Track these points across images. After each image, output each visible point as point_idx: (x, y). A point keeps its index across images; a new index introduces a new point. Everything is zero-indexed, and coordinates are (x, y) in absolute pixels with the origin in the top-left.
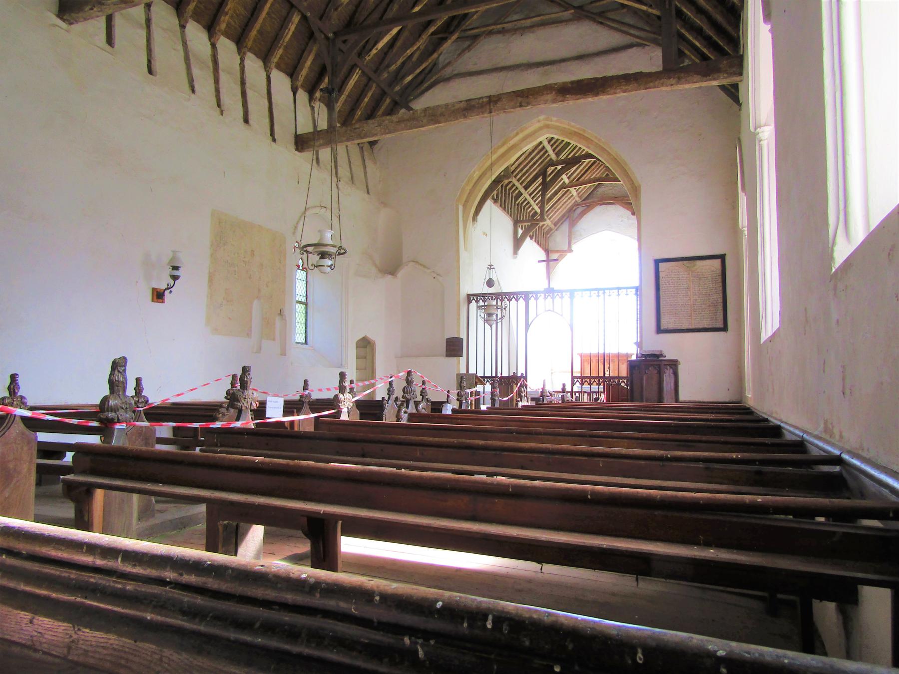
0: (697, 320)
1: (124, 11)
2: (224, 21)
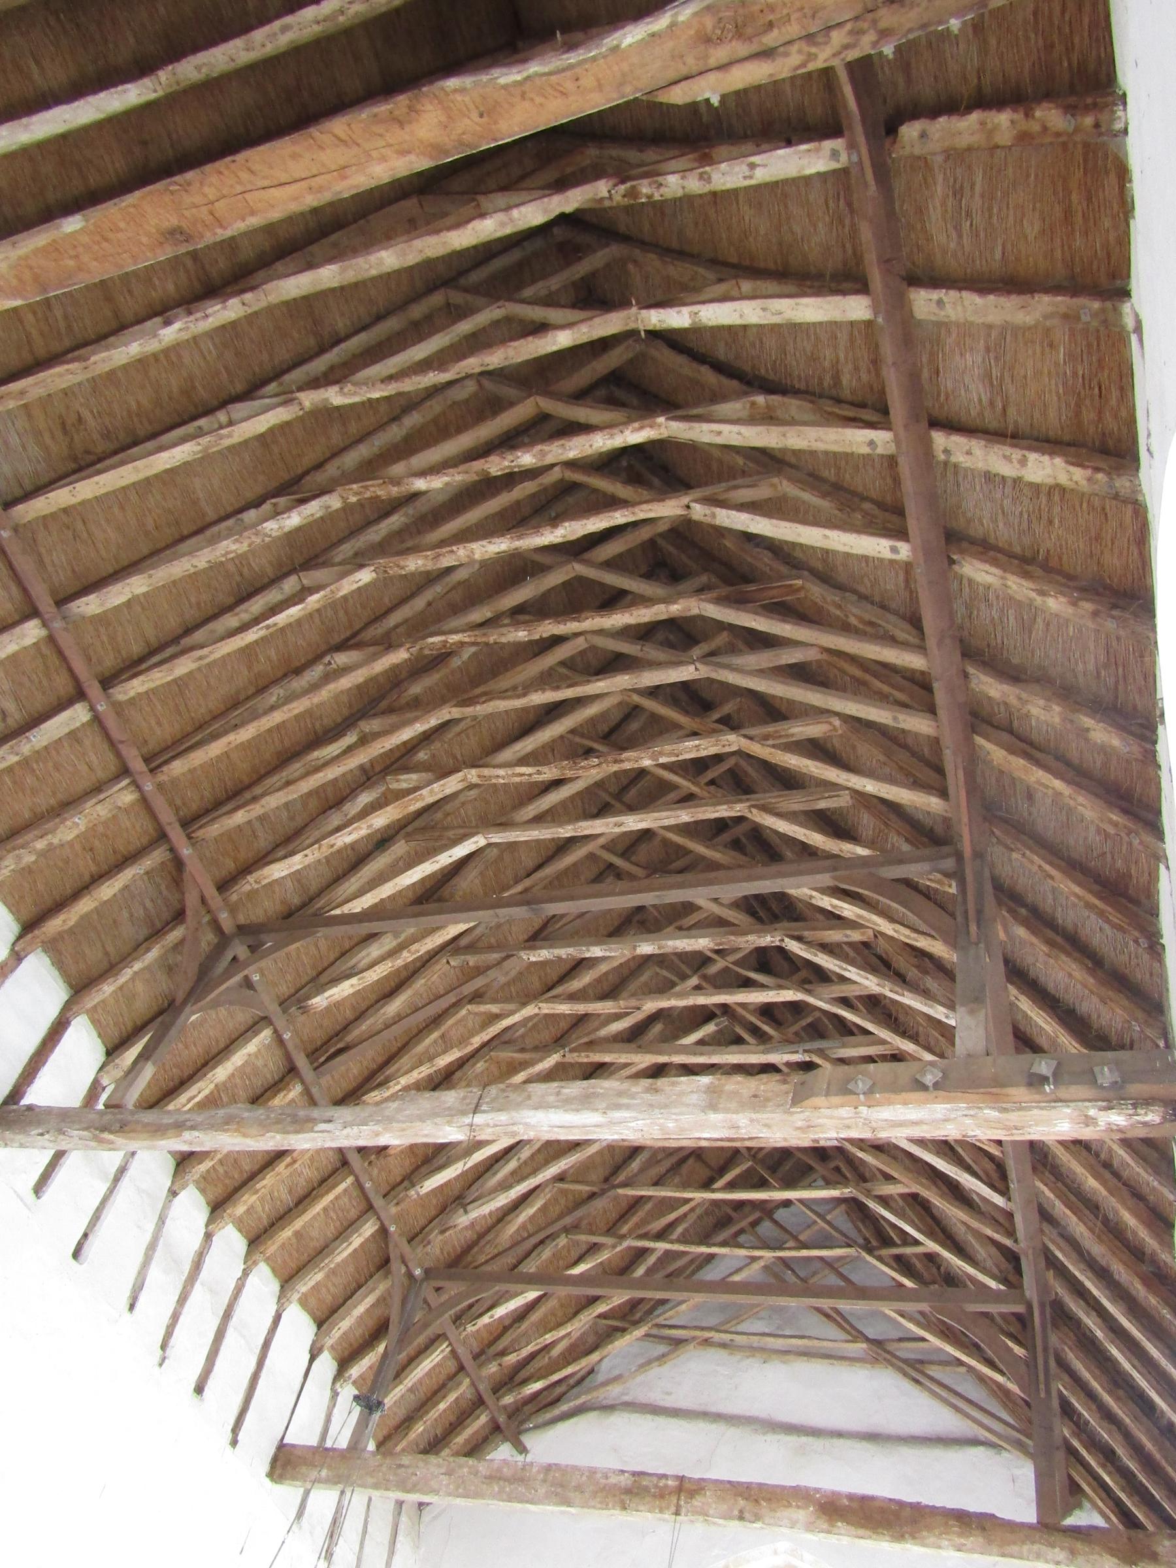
1: (91, 1153)
2: (245, 1202)
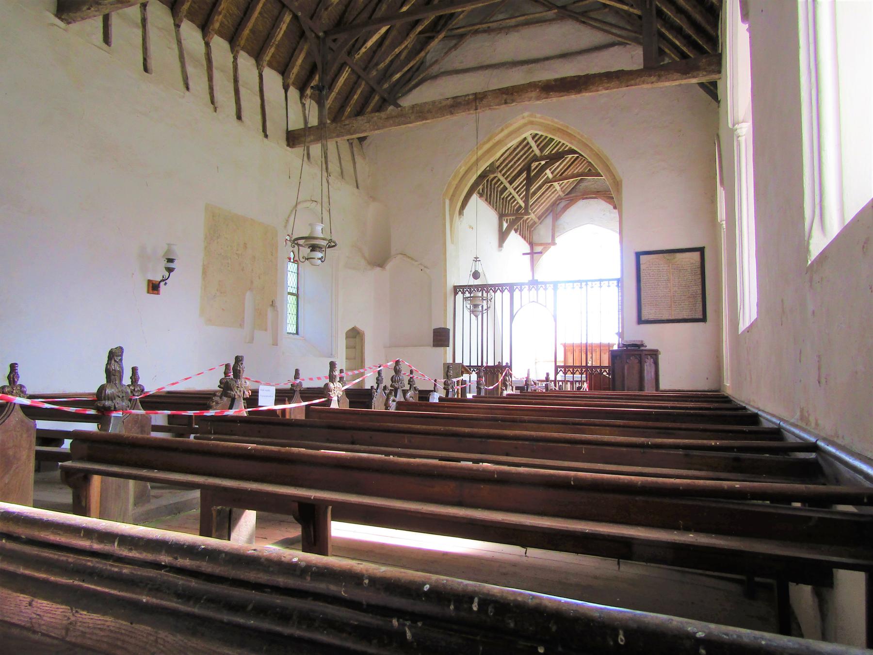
0: (677, 311)
1: (120, 11)
2: (217, 21)
